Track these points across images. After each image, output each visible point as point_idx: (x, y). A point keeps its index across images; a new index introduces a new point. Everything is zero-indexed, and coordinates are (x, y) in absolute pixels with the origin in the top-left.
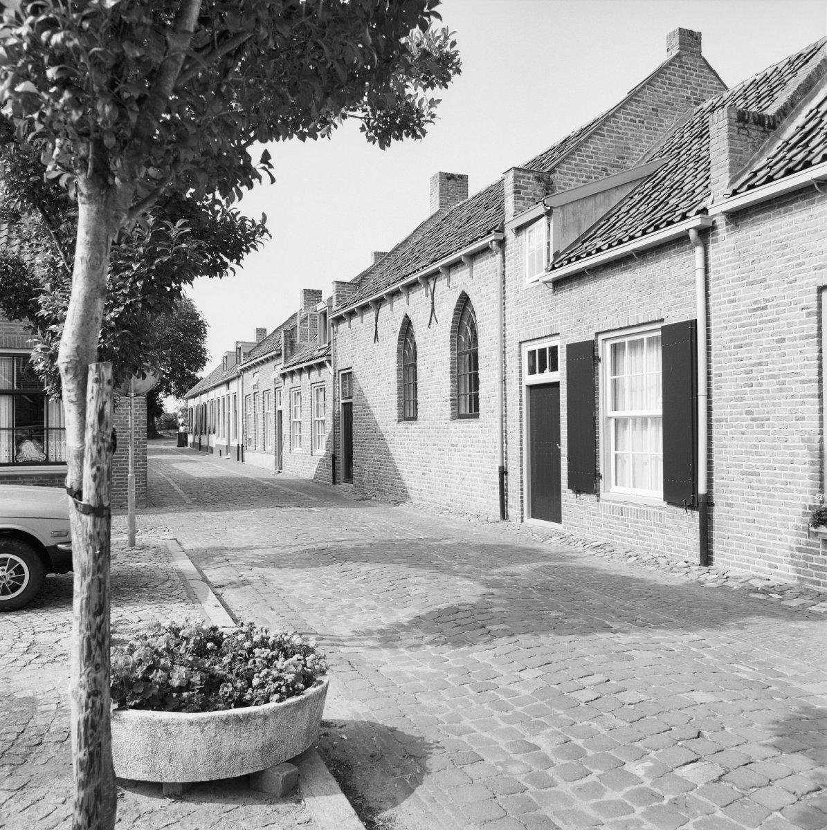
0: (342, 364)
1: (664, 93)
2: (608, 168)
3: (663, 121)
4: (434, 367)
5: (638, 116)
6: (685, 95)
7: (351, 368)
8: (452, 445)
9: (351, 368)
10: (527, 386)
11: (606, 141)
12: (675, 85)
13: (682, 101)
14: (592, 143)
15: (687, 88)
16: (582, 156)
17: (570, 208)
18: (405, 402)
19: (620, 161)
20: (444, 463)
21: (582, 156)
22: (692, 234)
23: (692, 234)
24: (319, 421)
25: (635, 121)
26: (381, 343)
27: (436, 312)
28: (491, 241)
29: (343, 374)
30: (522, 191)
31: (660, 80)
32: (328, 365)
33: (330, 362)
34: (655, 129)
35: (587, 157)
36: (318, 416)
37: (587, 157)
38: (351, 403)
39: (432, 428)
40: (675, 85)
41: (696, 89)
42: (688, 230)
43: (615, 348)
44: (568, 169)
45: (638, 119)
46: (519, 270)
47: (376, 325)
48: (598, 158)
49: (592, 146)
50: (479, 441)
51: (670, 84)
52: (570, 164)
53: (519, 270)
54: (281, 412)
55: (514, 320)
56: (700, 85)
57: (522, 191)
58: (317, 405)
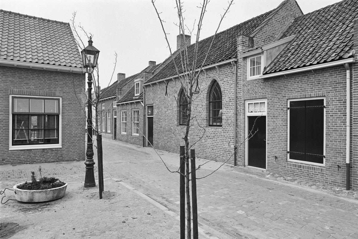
0: (149, 102)
1: (285, 12)
2: (270, 37)
3: (285, 22)
4: (197, 106)
5: (278, 20)
6: (291, 14)
7: (153, 104)
8: (207, 136)
9: (153, 104)
10: (247, 116)
11: (269, 27)
12: (288, 10)
13: (290, 16)
14: (265, 27)
15: (291, 11)
16: (263, 32)
17: (269, 51)
18: (209, 118)
19: (273, 35)
20: (202, 142)
21: (263, 32)
22: (346, 65)
23: (346, 65)
24: (123, 123)
25: (277, 21)
26: (168, 95)
27: (199, 86)
28: (232, 61)
29: (148, 106)
30: (245, 43)
31: (284, 7)
32: (141, 103)
33: (142, 102)
34: (283, 25)
35: (264, 32)
36: (123, 121)
37: (264, 32)
38: (153, 117)
39: (196, 129)
40: (288, 10)
41: (294, 12)
42: (345, 64)
43: (134, 111)
44: (258, 36)
45: (278, 21)
46: (245, 73)
47: (166, 89)
48: (267, 33)
49: (265, 29)
50: (222, 136)
51: (287, 9)
52: (259, 34)
53: (245, 73)
54: (115, 119)
55: (242, 91)
56: (295, 11)
57: (245, 43)
58: (123, 117)
